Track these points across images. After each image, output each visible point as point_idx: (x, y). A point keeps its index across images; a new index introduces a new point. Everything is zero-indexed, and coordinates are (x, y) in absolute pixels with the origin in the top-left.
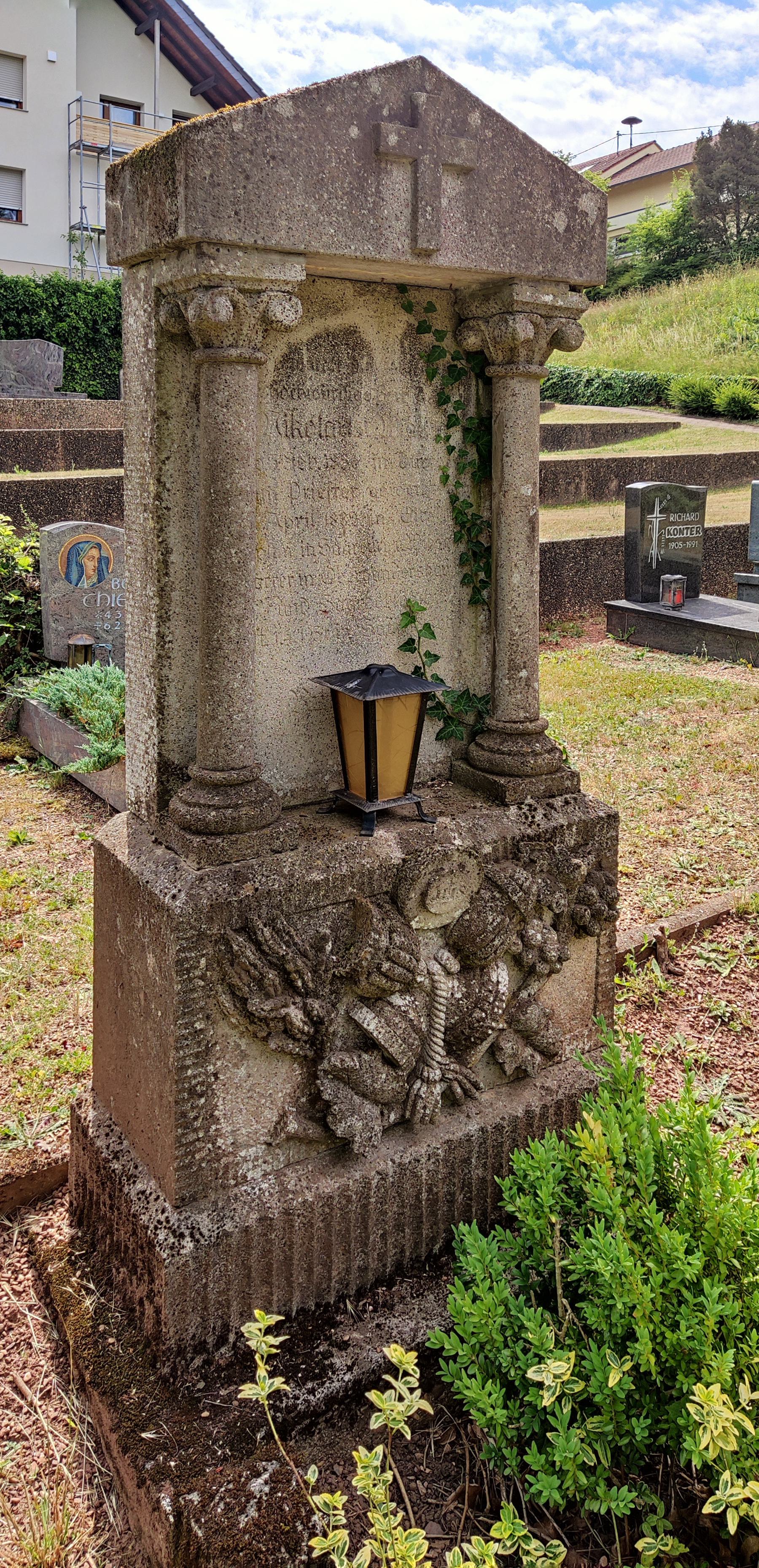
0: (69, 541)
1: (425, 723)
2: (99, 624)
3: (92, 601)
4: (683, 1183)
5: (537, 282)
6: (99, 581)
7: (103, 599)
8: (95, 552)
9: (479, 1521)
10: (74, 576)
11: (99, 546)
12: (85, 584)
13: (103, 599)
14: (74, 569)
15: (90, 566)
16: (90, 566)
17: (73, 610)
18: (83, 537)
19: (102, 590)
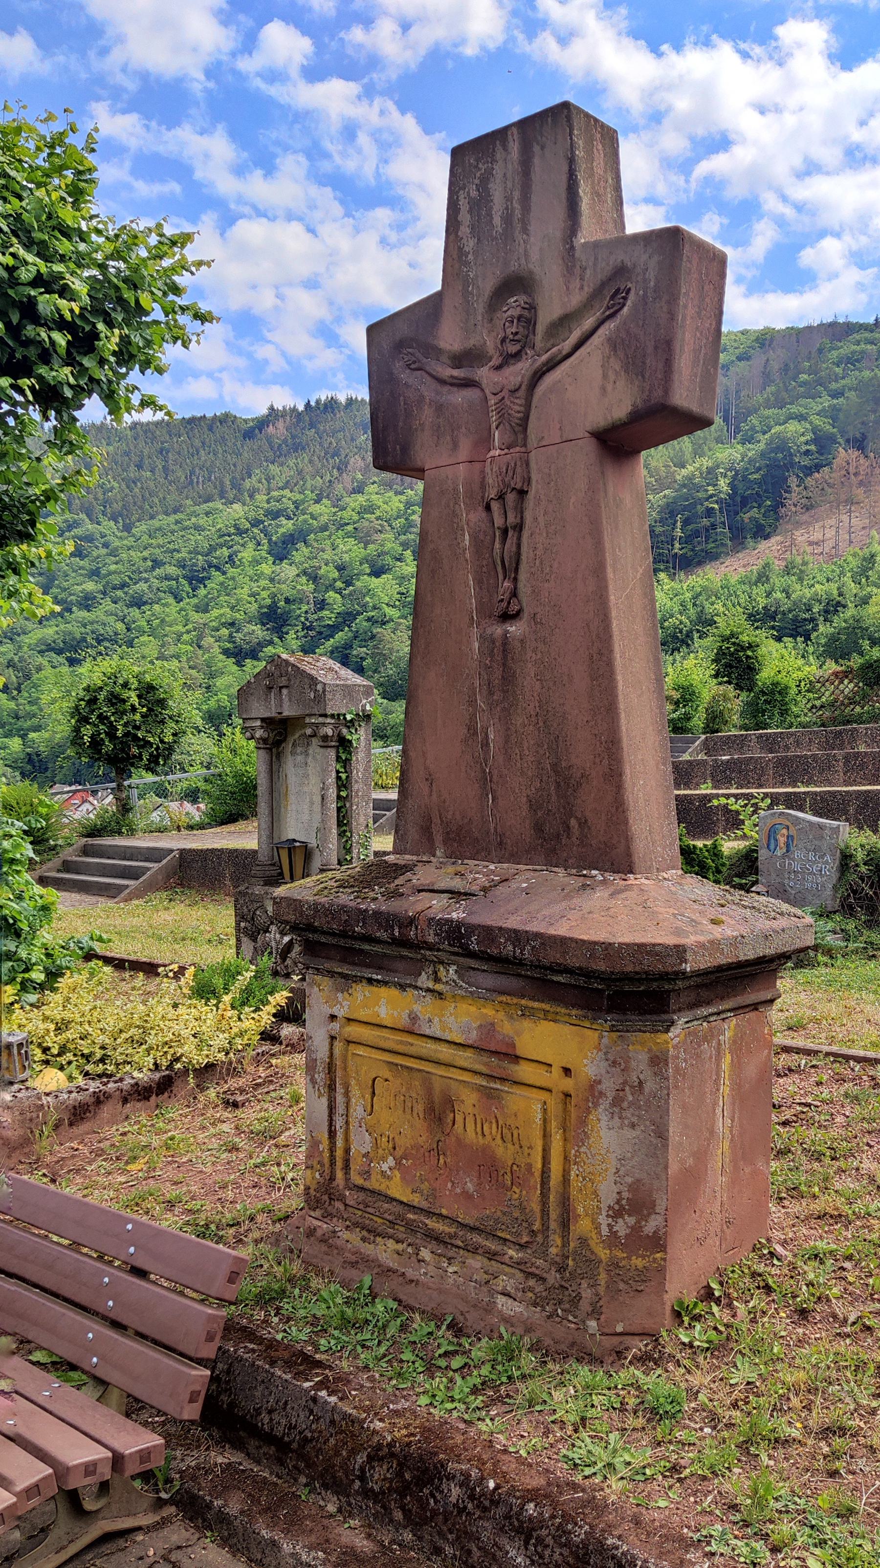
0: (769, 823)
1: (536, 161)
2: (786, 881)
3: (783, 865)
4: (257, 1196)
5: (310, 715)
6: (788, 851)
7: (790, 864)
8: (785, 831)
9: (25, 396)
10: (772, 847)
11: (788, 828)
12: (779, 853)
13: (790, 864)
14: (772, 841)
15: (782, 840)
16: (782, 840)
17: (772, 870)
18: (778, 821)
19: (790, 859)
